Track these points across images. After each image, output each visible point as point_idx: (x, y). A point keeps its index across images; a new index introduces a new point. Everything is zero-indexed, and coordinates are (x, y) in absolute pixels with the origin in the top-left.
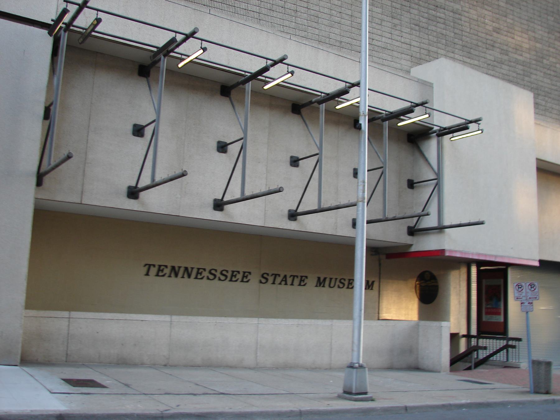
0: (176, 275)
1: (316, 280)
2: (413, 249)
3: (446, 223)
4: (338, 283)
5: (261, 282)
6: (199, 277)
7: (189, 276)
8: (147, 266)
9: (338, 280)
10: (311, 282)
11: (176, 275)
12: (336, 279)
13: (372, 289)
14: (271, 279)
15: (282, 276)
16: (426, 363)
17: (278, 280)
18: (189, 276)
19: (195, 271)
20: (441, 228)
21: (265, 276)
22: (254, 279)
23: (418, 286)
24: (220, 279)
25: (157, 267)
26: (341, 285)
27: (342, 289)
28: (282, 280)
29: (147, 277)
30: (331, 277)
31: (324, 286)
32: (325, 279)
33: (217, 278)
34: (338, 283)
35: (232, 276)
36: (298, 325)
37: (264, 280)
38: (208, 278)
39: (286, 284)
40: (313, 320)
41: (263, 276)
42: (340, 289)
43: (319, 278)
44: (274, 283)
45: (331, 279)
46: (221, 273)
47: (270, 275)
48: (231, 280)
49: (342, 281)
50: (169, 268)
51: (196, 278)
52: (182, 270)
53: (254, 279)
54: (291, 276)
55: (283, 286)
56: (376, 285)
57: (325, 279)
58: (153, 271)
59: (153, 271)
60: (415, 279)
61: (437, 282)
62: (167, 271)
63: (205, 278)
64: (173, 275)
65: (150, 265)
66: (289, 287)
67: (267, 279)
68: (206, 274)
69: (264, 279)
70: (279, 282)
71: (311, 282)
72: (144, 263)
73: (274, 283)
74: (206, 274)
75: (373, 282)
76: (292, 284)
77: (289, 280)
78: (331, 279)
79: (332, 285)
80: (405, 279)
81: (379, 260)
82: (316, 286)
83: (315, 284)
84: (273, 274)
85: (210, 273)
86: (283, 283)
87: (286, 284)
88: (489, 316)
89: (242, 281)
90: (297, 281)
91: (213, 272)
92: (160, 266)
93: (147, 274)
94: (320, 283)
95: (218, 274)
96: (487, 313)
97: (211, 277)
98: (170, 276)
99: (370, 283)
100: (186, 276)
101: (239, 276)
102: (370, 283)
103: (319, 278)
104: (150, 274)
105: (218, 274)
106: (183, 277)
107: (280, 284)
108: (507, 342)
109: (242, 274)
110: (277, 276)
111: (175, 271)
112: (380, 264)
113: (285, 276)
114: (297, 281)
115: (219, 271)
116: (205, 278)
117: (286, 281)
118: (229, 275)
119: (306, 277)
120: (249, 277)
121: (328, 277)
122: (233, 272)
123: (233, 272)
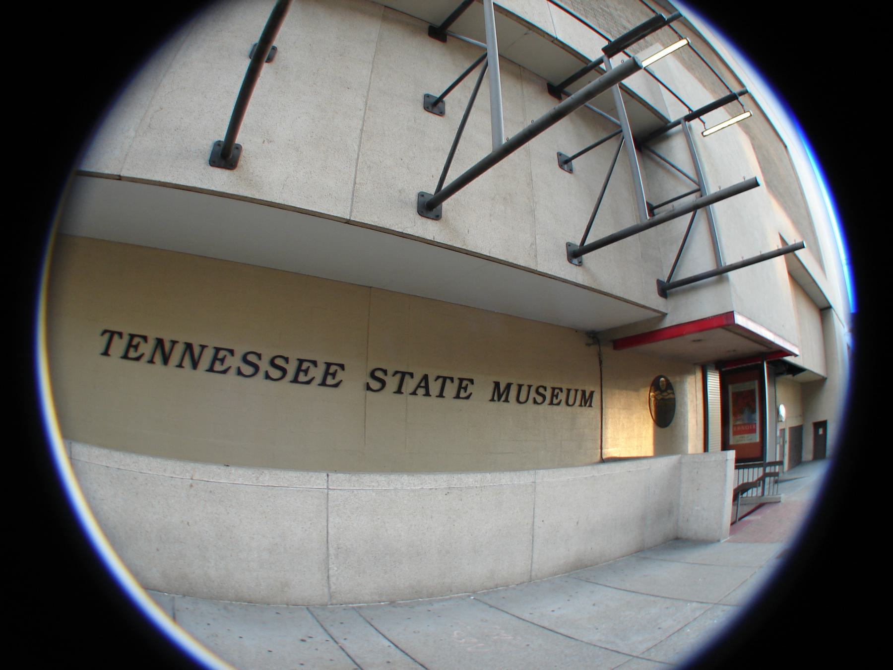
0: (166, 360)
1: (493, 385)
2: (668, 323)
3: (729, 259)
4: (533, 394)
5: (369, 388)
6: (218, 367)
7: (195, 365)
8: (107, 335)
9: (533, 390)
10: (482, 391)
11: (166, 360)
12: (530, 387)
13: (590, 406)
14: (392, 383)
15: (418, 377)
16: (695, 528)
17: (410, 384)
18: (195, 365)
19: (208, 355)
20: (720, 273)
21: (379, 374)
22: (353, 381)
23: (653, 399)
24: (267, 376)
25: (126, 338)
26: (539, 399)
27: (540, 406)
28: (419, 386)
29: (105, 358)
30: (521, 383)
31: (506, 400)
32: (509, 386)
33: (261, 374)
34: (533, 394)
35: (299, 370)
36: (449, 491)
37: (375, 385)
38: (239, 373)
39: (427, 394)
40: (488, 476)
41: (373, 375)
42: (536, 406)
43: (497, 385)
44: (399, 391)
45: (520, 386)
46: (272, 363)
47: (390, 373)
48: (295, 380)
49: (541, 390)
50: (152, 343)
51: (211, 370)
52: (179, 349)
53: (353, 381)
54: (438, 377)
55: (420, 397)
56: (596, 398)
57: (509, 386)
58: (119, 346)
59: (119, 346)
60: (649, 389)
61: (673, 393)
62: (146, 349)
63: (233, 371)
64: (158, 358)
65: (113, 333)
66: (433, 400)
67: (383, 383)
68: (234, 362)
69: (377, 379)
70: (411, 390)
71: (482, 391)
72: (101, 330)
73: (399, 391)
74: (234, 362)
75: (592, 393)
76: (441, 395)
77: (434, 387)
78: (520, 386)
79: (522, 398)
80: (636, 390)
81: (600, 356)
82: (492, 400)
83: (490, 397)
84: (396, 373)
85: (245, 360)
86: (421, 391)
87: (427, 394)
88: (738, 437)
89: (323, 383)
90: (451, 389)
91: (252, 358)
92: (132, 336)
93: (106, 353)
94: (500, 393)
95: (264, 365)
96: (735, 433)
97: (247, 370)
98: (151, 361)
99: (587, 395)
100: (187, 362)
101: (317, 373)
102: (587, 395)
103: (497, 385)
104: (111, 352)
105: (264, 365)
106: (180, 366)
107: (414, 393)
108: (764, 470)
109: (322, 368)
110: (407, 377)
111: (163, 351)
112: (601, 362)
113: (426, 378)
114: (451, 389)
115: (266, 359)
116: (233, 371)
117: (427, 387)
118: (291, 369)
119: (472, 381)
120: (340, 375)
121: (515, 382)
122: (301, 361)
123: (301, 361)
